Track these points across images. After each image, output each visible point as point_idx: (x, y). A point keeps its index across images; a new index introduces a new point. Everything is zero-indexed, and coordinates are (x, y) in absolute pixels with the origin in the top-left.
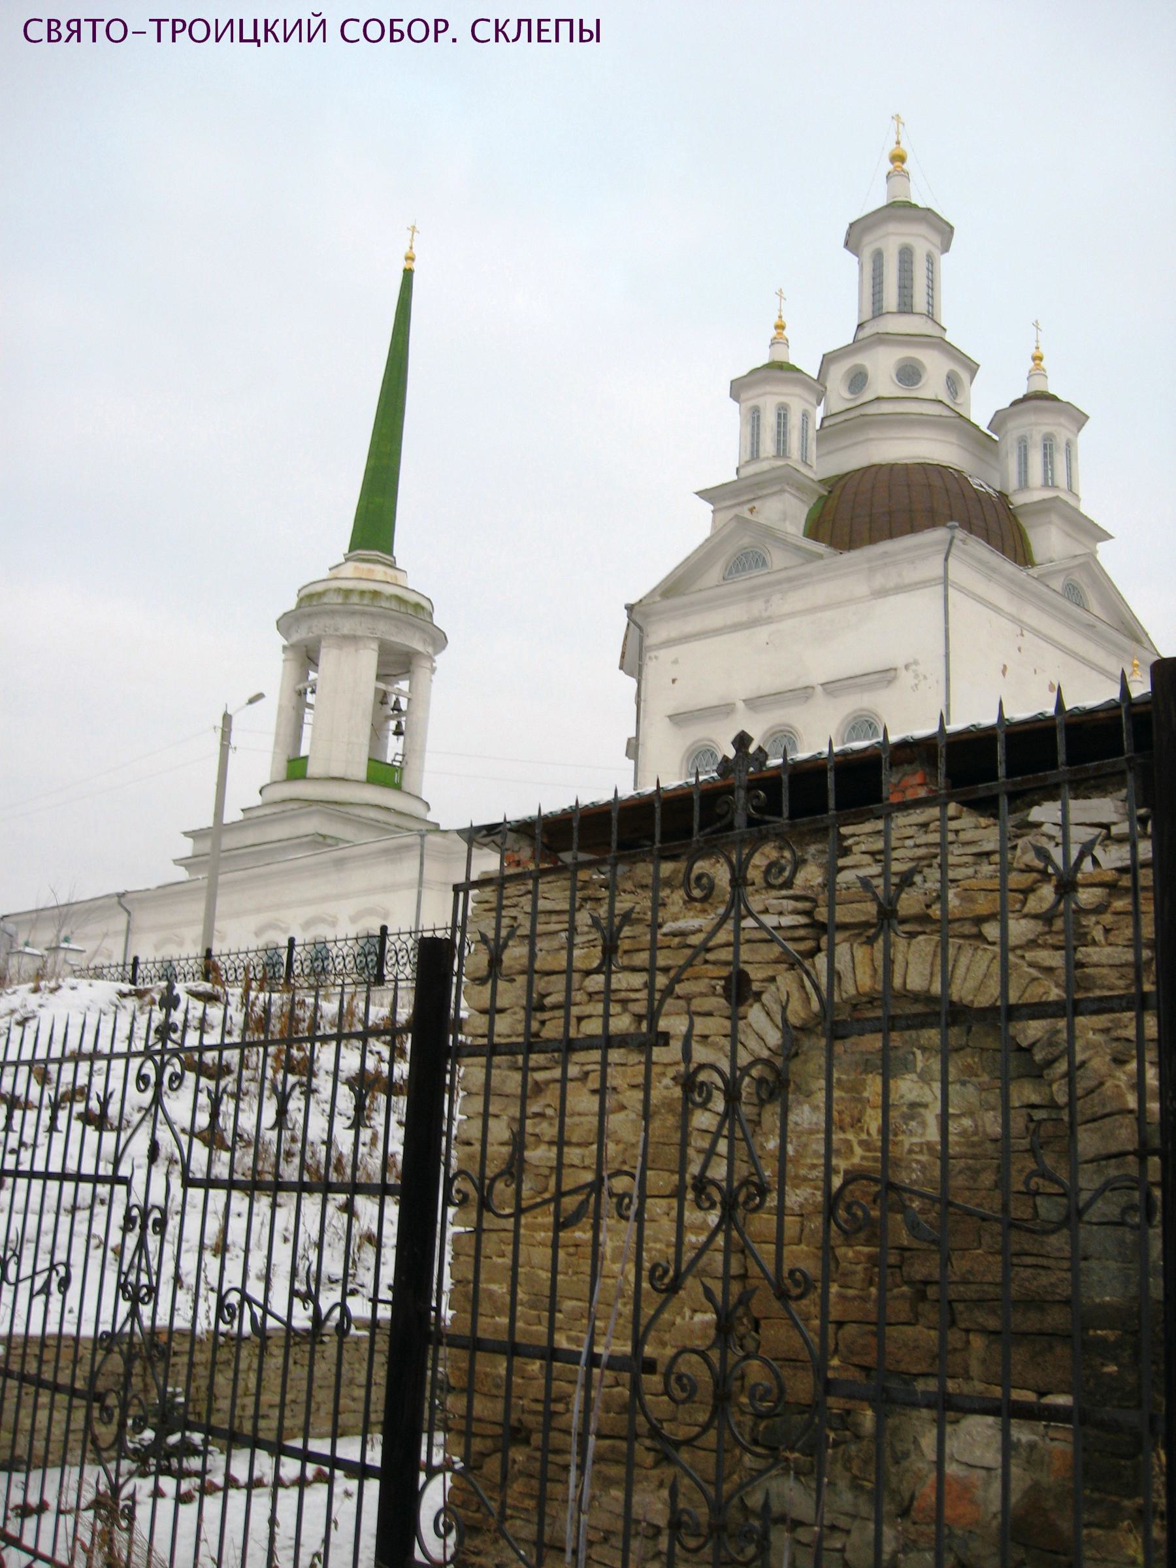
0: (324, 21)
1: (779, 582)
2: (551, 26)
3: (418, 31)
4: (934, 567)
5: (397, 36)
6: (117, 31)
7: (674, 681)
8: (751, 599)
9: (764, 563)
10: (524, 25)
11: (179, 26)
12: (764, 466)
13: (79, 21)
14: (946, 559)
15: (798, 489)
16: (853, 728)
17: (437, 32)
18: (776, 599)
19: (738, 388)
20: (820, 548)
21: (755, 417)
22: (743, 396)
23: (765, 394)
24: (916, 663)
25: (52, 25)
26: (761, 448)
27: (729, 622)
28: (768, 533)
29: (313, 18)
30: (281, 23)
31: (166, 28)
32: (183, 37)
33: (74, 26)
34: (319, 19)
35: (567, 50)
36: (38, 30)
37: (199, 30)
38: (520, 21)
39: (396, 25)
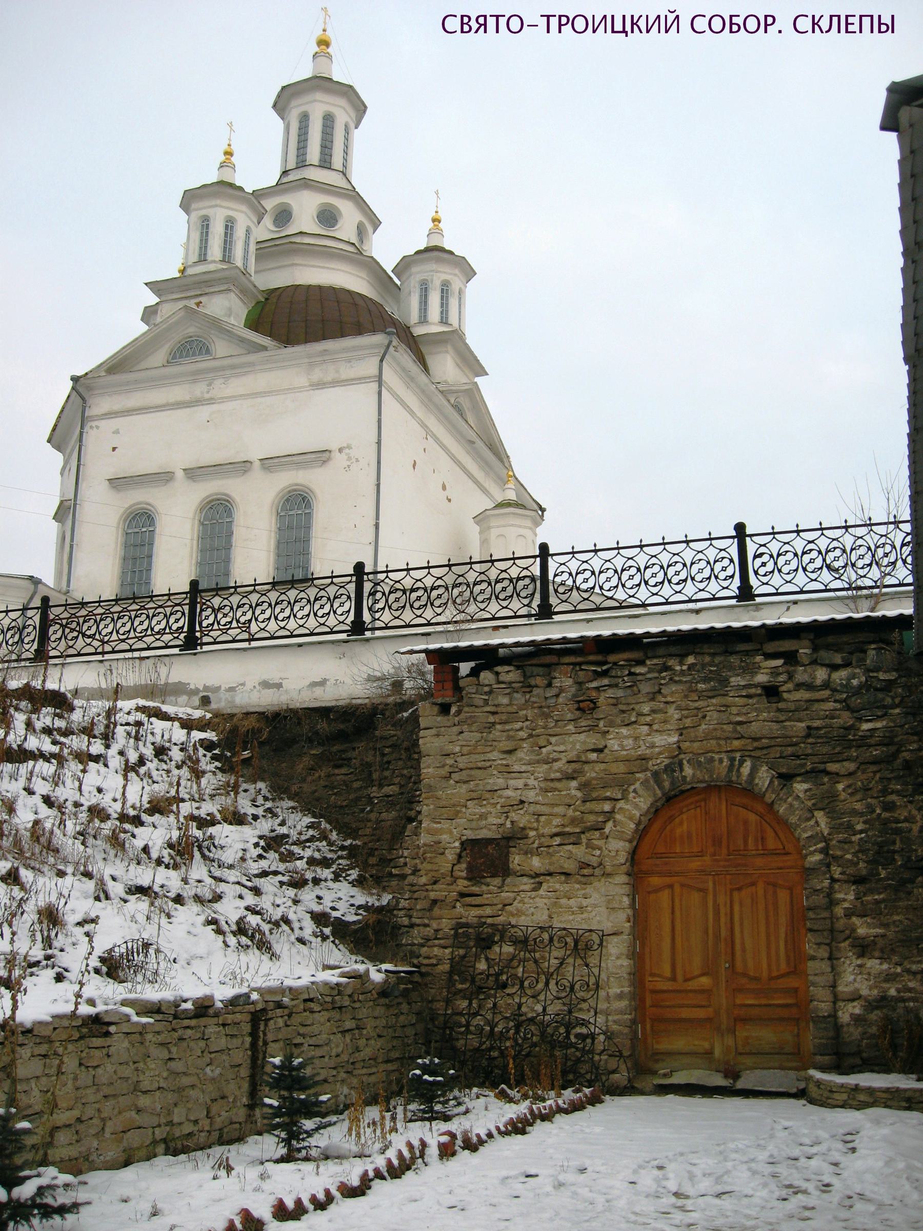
0: (677, 17)
1: (222, 368)
2: (856, 20)
3: (752, 24)
4: (369, 367)
5: (735, 28)
6: (515, 24)
7: (114, 449)
8: (195, 381)
9: (208, 352)
10: (835, 20)
11: (564, 20)
12: (212, 267)
13: (485, 17)
14: (381, 361)
15: (242, 291)
16: (287, 500)
17: (766, 25)
18: (218, 383)
19: (189, 199)
20: (265, 341)
21: (205, 224)
22: (193, 206)
23: (217, 206)
24: (349, 447)
25: (464, 20)
26: (209, 252)
27: (172, 400)
28: (215, 324)
29: (669, 15)
30: (644, 18)
31: (554, 22)
32: (567, 29)
33: (481, 20)
34: (674, 15)
35: (868, 39)
36: (453, 24)
37: (580, 24)
38: (831, 17)
39: (735, 20)
